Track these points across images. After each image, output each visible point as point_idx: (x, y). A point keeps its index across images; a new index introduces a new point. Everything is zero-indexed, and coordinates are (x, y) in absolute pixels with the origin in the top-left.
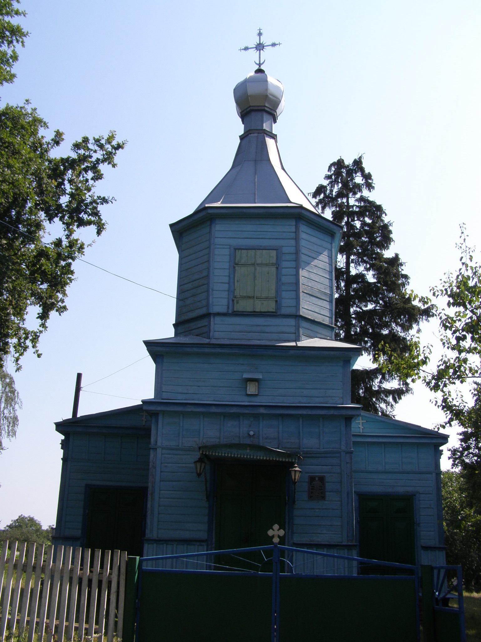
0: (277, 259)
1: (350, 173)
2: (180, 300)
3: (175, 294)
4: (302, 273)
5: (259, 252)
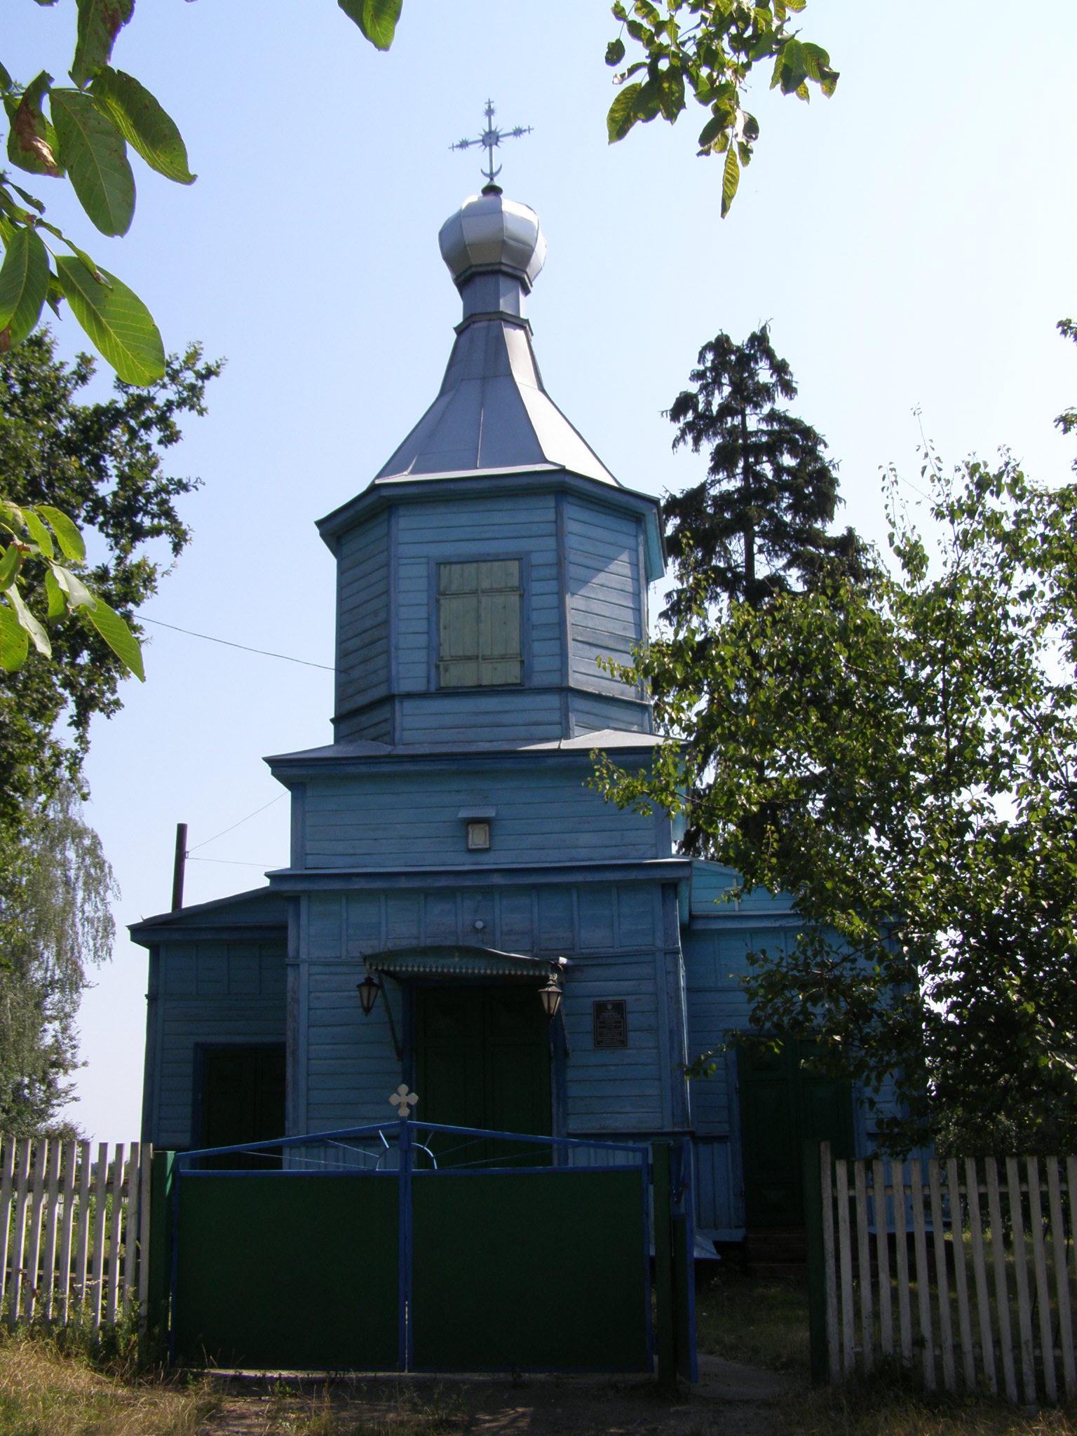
0: (521, 578)
4: (571, 602)
5: (484, 567)
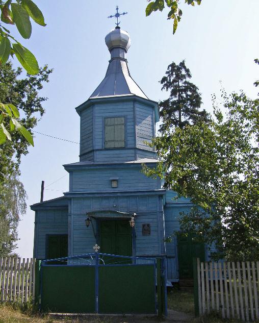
1: (179, 69)
2: (82, 144)
3: (79, 141)
4: (137, 127)
